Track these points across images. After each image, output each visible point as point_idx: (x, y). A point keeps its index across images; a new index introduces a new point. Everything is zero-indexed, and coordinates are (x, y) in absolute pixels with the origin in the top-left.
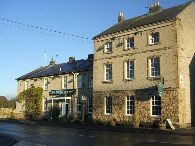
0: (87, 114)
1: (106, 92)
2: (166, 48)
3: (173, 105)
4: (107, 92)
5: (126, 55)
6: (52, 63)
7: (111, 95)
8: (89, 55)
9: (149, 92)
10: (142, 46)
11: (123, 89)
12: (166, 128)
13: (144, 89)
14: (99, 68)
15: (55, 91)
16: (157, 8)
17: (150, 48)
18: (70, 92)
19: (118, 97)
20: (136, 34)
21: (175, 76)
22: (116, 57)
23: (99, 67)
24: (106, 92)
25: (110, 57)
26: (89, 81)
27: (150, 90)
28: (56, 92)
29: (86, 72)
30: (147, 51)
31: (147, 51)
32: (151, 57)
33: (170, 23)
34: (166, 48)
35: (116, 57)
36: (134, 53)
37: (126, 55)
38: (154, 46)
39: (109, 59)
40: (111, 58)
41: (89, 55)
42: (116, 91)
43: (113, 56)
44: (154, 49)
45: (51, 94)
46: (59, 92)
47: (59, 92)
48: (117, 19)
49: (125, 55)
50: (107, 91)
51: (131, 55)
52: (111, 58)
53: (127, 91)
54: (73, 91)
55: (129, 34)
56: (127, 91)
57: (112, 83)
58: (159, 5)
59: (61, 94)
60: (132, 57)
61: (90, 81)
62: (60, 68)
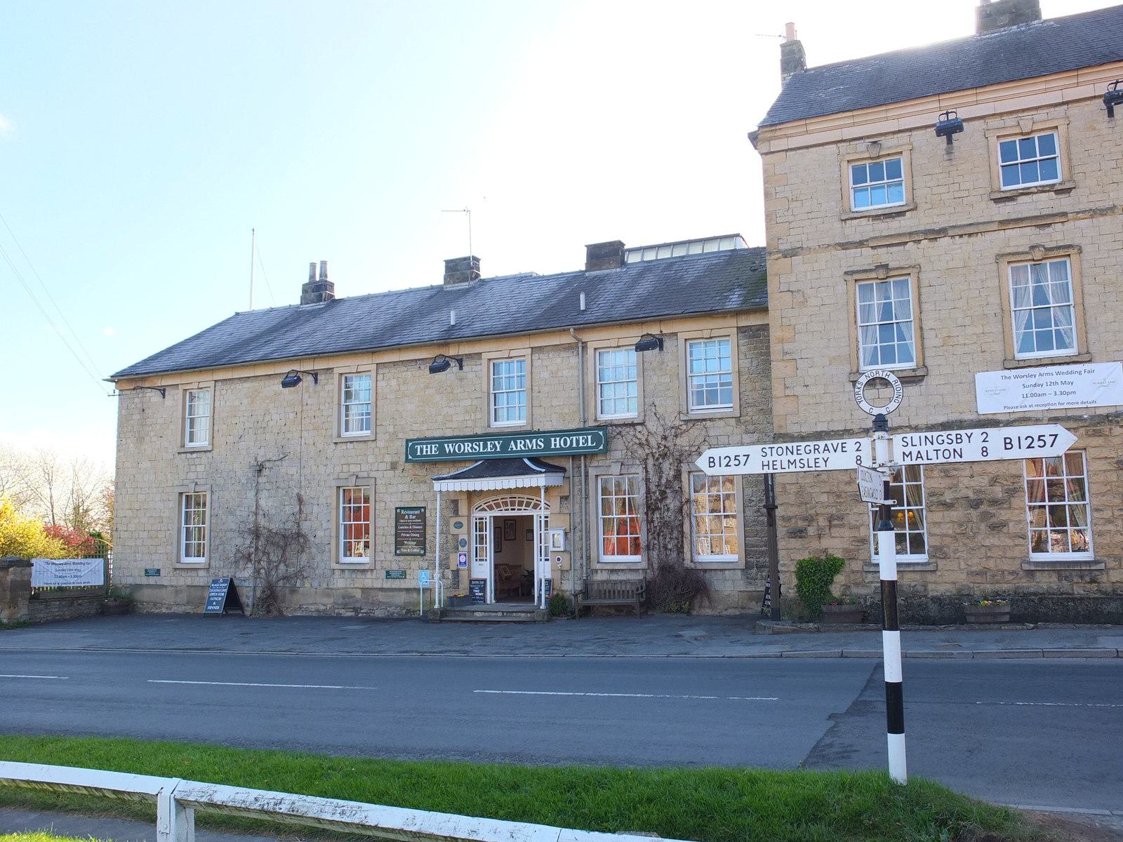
0: (693, 566)
5: (1005, 223)
6: (318, 289)
8: (447, 262)
15: (441, 441)
18: (556, 443)
22: (935, 234)
23: (809, 292)
26: (188, 422)
28: (449, 448)
29: (320, 365)
30: (844, 246)
31: (844, 246)
35: (935, 234)
36: (1065, 214)
37: (1005, 223)
39: (880, 251)
40: (898, 241)
41: (447, 262)
43: (917, 233)
46: (467, 448)
47: (467, 448)
48: (777, 56)
49: (1001, 222)
51: (1042, 221)
52: (898, 241)
55: (1023, 110)
57: (921, 381)
59: (486, 460)
61: (347, 407)
62: (582, 297)
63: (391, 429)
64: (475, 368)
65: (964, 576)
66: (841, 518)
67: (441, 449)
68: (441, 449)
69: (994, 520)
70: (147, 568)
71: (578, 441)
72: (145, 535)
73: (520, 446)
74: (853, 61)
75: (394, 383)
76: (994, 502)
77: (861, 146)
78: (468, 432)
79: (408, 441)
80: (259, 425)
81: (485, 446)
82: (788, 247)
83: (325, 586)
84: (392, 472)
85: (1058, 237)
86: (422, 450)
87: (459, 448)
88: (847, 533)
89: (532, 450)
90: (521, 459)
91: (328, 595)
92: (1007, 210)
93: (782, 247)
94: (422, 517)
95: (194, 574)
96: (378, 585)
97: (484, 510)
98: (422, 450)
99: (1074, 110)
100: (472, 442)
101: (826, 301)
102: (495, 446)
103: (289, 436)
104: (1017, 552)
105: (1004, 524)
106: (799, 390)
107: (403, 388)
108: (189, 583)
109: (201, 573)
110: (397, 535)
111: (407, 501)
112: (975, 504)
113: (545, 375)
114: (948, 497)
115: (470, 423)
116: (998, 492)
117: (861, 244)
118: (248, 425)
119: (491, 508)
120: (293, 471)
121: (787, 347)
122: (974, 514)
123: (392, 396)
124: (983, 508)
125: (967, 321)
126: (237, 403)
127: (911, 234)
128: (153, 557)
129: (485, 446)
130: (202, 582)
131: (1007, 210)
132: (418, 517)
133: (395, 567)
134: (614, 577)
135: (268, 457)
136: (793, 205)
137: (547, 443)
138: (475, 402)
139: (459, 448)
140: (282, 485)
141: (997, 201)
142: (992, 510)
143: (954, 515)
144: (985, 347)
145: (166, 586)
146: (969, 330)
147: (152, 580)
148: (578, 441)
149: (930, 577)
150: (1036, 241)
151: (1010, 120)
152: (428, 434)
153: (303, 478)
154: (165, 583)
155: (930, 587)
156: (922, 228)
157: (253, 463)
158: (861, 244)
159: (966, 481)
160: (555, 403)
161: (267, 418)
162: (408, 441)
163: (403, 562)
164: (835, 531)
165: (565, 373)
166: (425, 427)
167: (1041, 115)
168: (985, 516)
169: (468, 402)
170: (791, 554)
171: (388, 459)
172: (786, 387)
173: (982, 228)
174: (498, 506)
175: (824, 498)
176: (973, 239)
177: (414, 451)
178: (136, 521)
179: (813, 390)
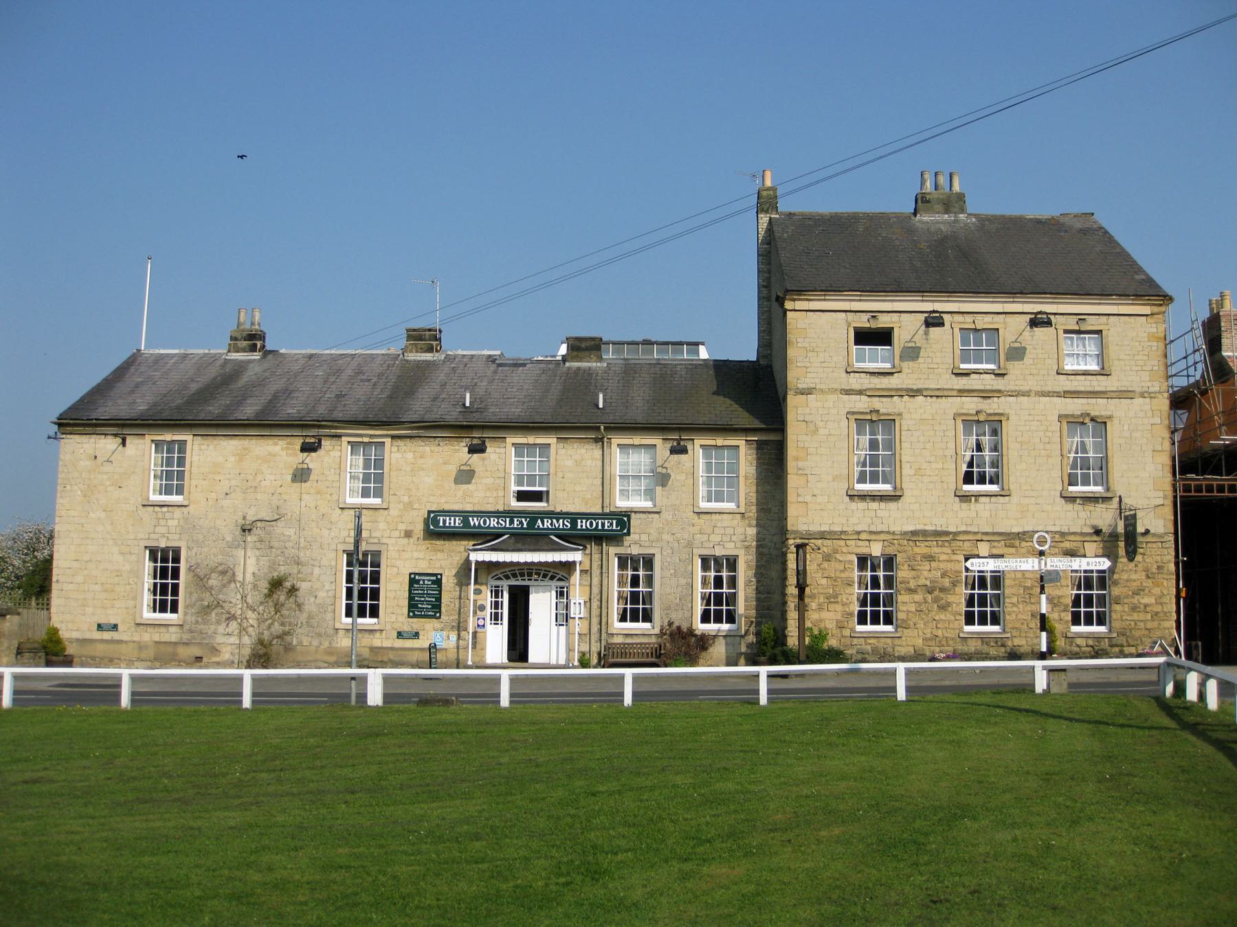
1: (863, 536)
2: (1130, 395)
3: (1157, 591)
4: (873, 537)
5: (962, 392)
7: (890, 551)
9: (1067, 545)
10: (1034, 371)
11: (952, 529)
12: (528, 587)
13: (99, 385)
14: (822, 431)
15: (465, 515)
16: (953, 203)
17: (1068, 383)
19: (930, 558)
20: (1038, 321)
21: (1161, 494)
22: (914, 393)
23: (820, 424)
24: (863, 536)
25: (883, 389)
27: (1072, 538)
28: (474, 521)
30: (848, 392)
31: (848, 392)
32: (1072, 416)
33: (1147, 310)
34: (1130, 395)
35: (914, 393)
36: (999, 391)
37: (962, 392)
38: (1083, 377)
40: (888, 394)
42: (915, 536)
44: (1082, 389)
45: (435, 530)
46: (493, 522)
47: (493, 522)
50: (871, 533)
51: (986, 395)
52: (888, 394)
53: (971, 537)
54: (610, 525)
56: (971, 537)
58: (957, 187)
59: (512, 535)
60: (993, 406)
63: (406, 499)
64: (498, 450)
65: (921, 641)
66: (836, 597)
67: (466, 522)
68: (466, 522)
69: (943, 602)
70: (101, 622)
71: (603, 525)
72: (97, 588)
73: (547, 524)
74: (821, 215)
75: (410, 456)
76: (942, 590)
77: (865, 317)
78: (490, 508)
79: (430, 512)
80: (249, 484)
81: (512, 522)
82: (805, 386)
83: (326, 644)
84: (406, 540)
85: (995, 406)
86: (444, 522)
87: (485, 522)
88: (839, 608)
89: (558, 529)
90: (547, 535)
91: (331, 654)
92: (962, 383)
93: (800, 386)
94: (438, 582)
95: (163, 629)
96: (387, 644)
97: (500, 579)
98: (444, 522)
99: (1010, 318)
100: (498, 518)
101: (833, 432)
102: (521, 523)
103: (286, 497)
104: (956, 624)
105: (949, 604)
106: (808, 498)
107: (420, 461)
108: (157, 639)
109: (172, 629)
110: (411, 598)
111: (423, 567)
112: (930, 591)
113: (570, 463)
114: (912, 584)
115: (491, 500)
116: (946, 582)
117: (860, 392)
118: (233, 483)
119: (507, 578)
120: (290, 532)
121: (800, 464)
122: (929, 597)
123: (409, 469)
124: (936, 593)
125: (933, 459)
126: (221, 459)
127: (897, 390)
128: (109, 612)
129: (512, 522)
130: (174, 638)
131: (962, 383)
132: (434, 582)
133: (406, 628)
134: (629, 640)
135: (260, 517)
136: (810, 354)
137: (574, 523)
138: (497, 481)
139: (485, 522)
140: (276, 545)
141: (957, 375)
142: (942, 595)
143: (918, 597)
144: (944, 479)
145: (126, 642)
146: (934, 466)
147: (107, 635)
148: (603, 525)
149: (897, 641)
150: (981, 407)
151: (969, 318)
152: (447, 508)
153: (302, 540)
154: (125, 637)
155: (897, 648)
156: (904, 386)
157: (241, 522)
158: (860, 392)
159: (925, 573)
160: (578, 488)
161: (259, 478)
162: (430, 512)
163: (416, 624)
164: (832, 607)
165: (589, 462)
166: (443, 500)
167: (988, 318)
168: (936, 600)
169: (490, 481)
170: (364, 547)
171: (402, 527)
172: (798, 495)
173: (946, 393)
174: (515, 576)
175: (824, 581)
176: (939, 400)
177: (436, 522)
178: (85, 572)
179: (819, 499)
